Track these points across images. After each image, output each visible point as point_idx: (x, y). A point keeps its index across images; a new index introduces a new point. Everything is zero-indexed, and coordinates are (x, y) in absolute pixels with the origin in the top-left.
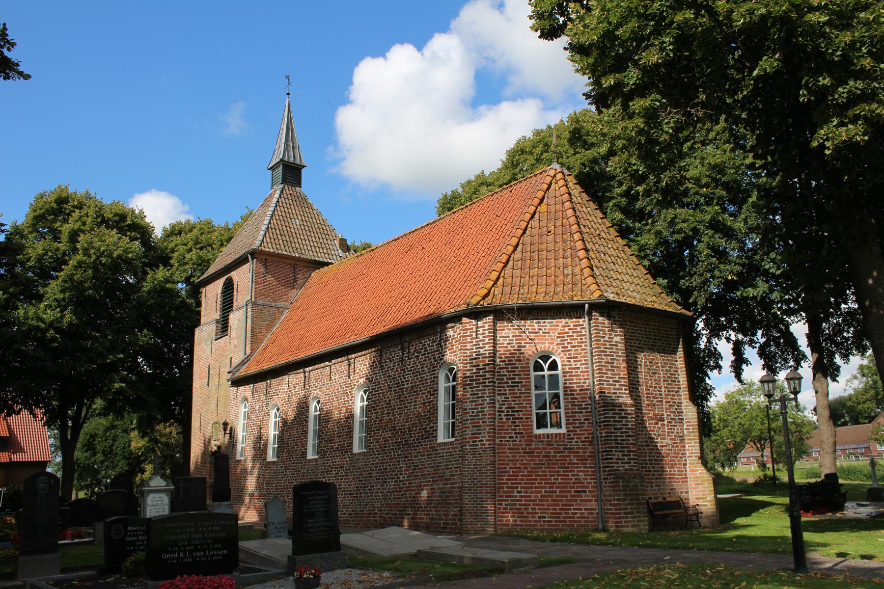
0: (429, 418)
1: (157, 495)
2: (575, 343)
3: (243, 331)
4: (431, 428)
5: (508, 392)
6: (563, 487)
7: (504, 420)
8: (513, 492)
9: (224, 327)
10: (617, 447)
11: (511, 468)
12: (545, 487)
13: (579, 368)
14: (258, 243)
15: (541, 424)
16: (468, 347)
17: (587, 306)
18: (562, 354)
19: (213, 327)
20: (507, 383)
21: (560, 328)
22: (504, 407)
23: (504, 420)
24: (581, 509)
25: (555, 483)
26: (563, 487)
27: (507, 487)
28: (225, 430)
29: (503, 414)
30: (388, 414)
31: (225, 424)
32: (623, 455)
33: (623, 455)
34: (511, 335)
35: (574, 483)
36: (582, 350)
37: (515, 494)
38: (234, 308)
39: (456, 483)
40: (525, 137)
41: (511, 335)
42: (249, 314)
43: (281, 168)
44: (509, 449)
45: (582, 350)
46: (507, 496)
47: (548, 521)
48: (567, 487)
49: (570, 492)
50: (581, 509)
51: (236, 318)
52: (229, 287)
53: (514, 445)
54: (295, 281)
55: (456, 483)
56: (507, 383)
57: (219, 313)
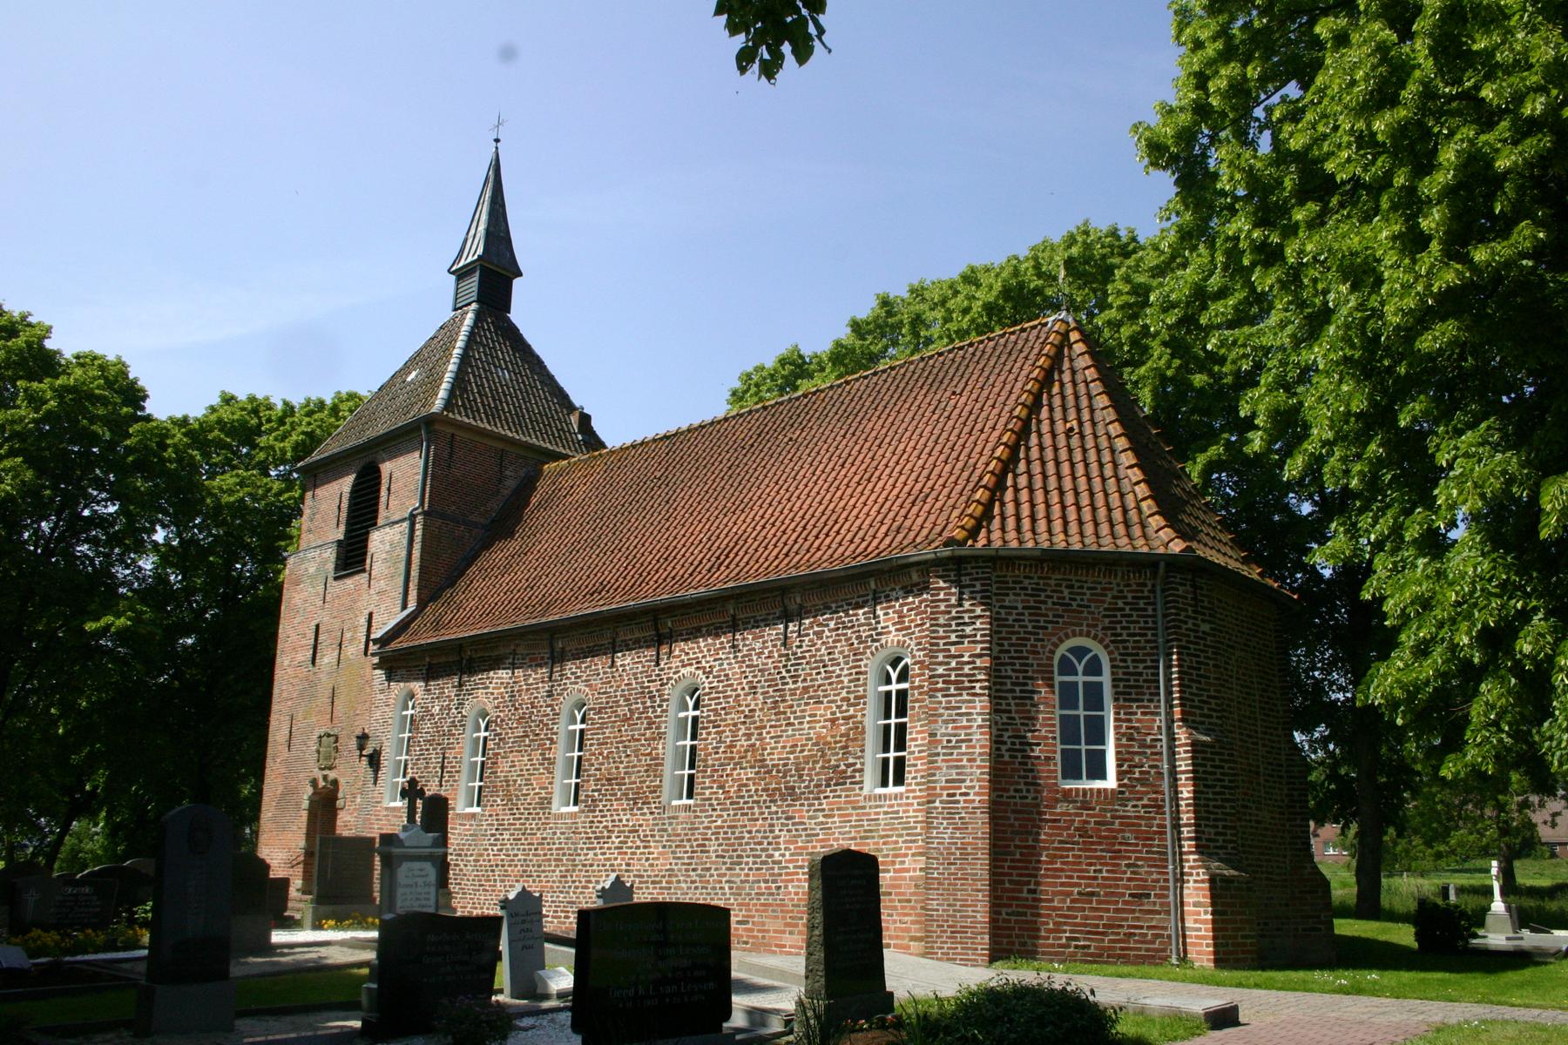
0: (846, 747)
1: (417, 865)
2: (1134, 629)
3: (402, 566)
4: (848, 766)
5: (1013, 708)
6: (1110, 886)
7: (1007, 758)
8: (1106, 894)
9: (352, 557)
10: (1208, 819)
11: (1017, 847)
12: (1078, 885)
13: (1140, 674)
14: (438, 404)
15: (1072, 771)
16: (941, 621)
17: (1162, 564)
18: (1112, 647)
19: (330, 555)
20: (1013, 691)
21: (1108, 599)
22: (1006, 734)
23: (1007, 758)
24: (1141, 927)
25: (1095, 878)
26: (1110, 886)
27: (1011, 882)
28: (361, 748)
29: (1004, 748)
30: (748, 736)
31: (363, 739)
32: (1217, 834)
33: (1217, 834)
34: (1020, 606)
35: (1129, 879)
36: (1148, 641)
37: (1025, 895)
38: (380, 522)
39: (907, 870)
40: (145, 397)
41: (1020, 606)
42: (418, 533)
43: (476, 278)
44: (1014, 812)
45: (1148, 641)
46: (1009, 898)
47: (1084, 947)
48: (1117, 886)
49: (1123, 895)
50: (1141, 927)
51: (386, 543)
53: (1022, 805)
54: (500, 481)
55: (907, 870)
56: (1013, 691)
57: (342, 528)
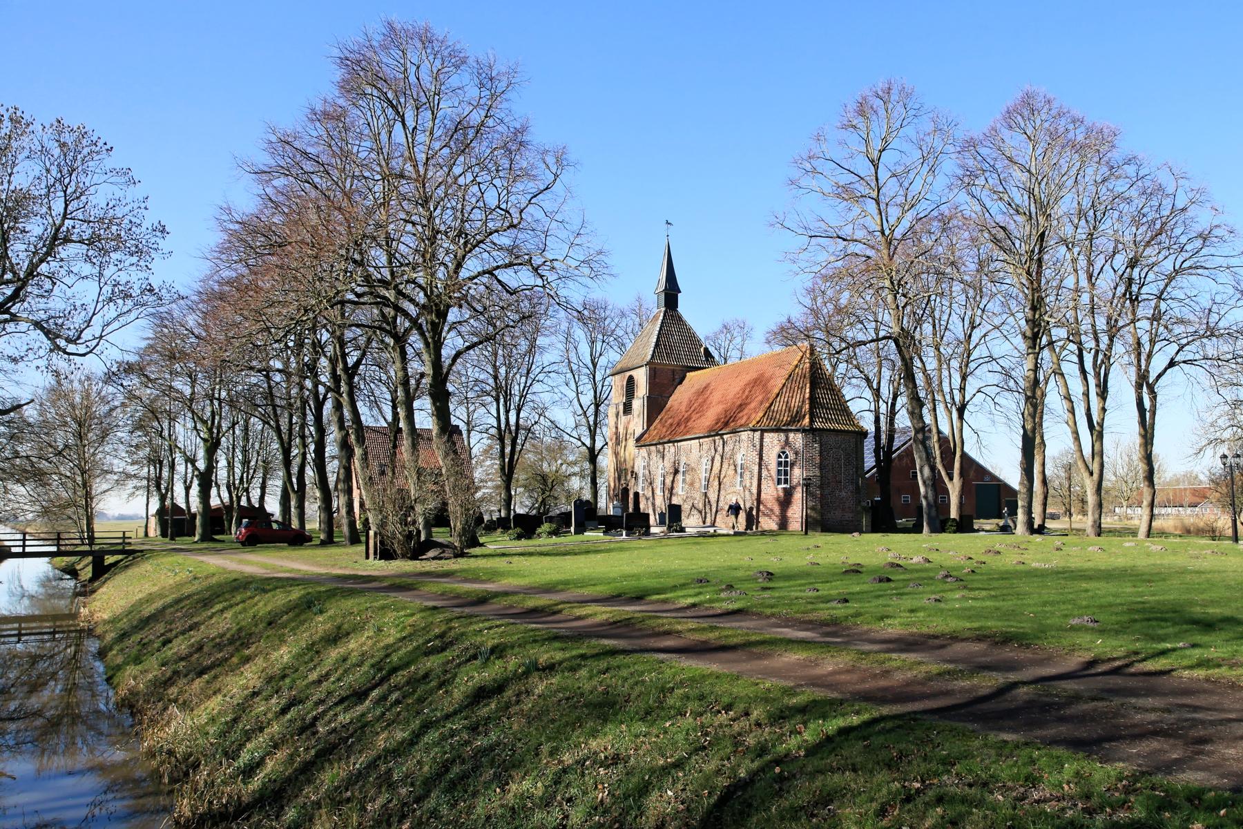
52: (631, 380)
